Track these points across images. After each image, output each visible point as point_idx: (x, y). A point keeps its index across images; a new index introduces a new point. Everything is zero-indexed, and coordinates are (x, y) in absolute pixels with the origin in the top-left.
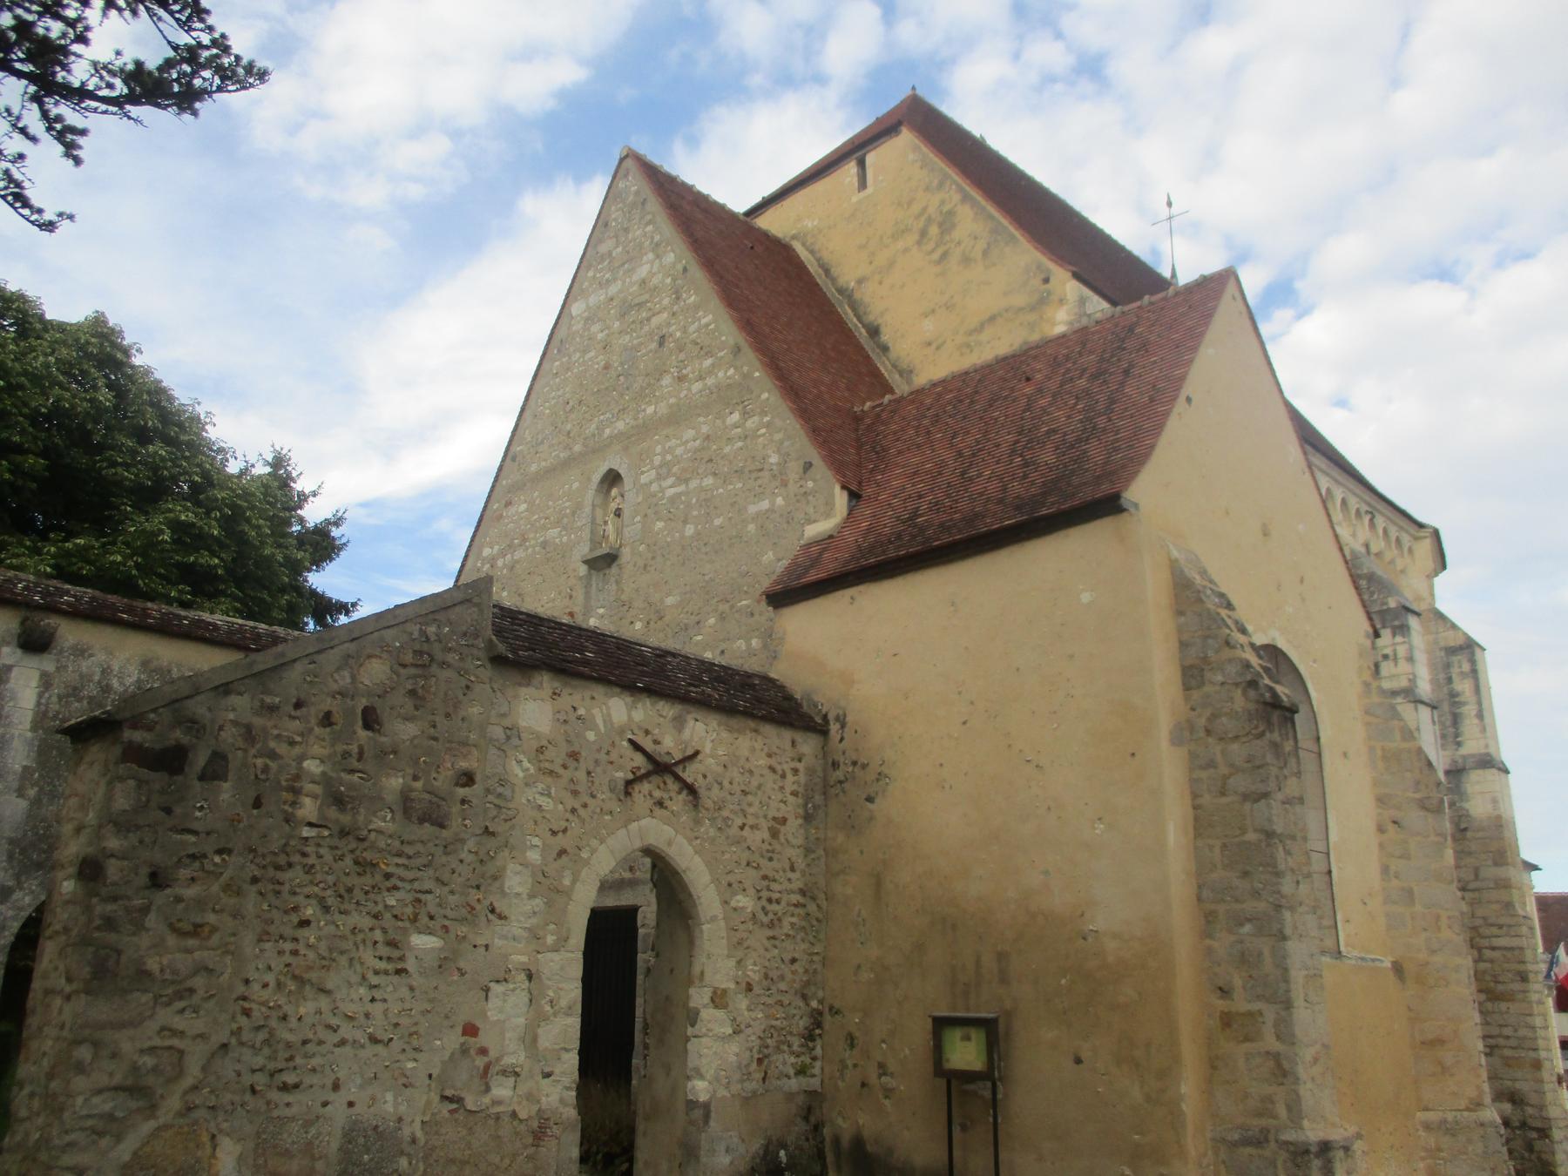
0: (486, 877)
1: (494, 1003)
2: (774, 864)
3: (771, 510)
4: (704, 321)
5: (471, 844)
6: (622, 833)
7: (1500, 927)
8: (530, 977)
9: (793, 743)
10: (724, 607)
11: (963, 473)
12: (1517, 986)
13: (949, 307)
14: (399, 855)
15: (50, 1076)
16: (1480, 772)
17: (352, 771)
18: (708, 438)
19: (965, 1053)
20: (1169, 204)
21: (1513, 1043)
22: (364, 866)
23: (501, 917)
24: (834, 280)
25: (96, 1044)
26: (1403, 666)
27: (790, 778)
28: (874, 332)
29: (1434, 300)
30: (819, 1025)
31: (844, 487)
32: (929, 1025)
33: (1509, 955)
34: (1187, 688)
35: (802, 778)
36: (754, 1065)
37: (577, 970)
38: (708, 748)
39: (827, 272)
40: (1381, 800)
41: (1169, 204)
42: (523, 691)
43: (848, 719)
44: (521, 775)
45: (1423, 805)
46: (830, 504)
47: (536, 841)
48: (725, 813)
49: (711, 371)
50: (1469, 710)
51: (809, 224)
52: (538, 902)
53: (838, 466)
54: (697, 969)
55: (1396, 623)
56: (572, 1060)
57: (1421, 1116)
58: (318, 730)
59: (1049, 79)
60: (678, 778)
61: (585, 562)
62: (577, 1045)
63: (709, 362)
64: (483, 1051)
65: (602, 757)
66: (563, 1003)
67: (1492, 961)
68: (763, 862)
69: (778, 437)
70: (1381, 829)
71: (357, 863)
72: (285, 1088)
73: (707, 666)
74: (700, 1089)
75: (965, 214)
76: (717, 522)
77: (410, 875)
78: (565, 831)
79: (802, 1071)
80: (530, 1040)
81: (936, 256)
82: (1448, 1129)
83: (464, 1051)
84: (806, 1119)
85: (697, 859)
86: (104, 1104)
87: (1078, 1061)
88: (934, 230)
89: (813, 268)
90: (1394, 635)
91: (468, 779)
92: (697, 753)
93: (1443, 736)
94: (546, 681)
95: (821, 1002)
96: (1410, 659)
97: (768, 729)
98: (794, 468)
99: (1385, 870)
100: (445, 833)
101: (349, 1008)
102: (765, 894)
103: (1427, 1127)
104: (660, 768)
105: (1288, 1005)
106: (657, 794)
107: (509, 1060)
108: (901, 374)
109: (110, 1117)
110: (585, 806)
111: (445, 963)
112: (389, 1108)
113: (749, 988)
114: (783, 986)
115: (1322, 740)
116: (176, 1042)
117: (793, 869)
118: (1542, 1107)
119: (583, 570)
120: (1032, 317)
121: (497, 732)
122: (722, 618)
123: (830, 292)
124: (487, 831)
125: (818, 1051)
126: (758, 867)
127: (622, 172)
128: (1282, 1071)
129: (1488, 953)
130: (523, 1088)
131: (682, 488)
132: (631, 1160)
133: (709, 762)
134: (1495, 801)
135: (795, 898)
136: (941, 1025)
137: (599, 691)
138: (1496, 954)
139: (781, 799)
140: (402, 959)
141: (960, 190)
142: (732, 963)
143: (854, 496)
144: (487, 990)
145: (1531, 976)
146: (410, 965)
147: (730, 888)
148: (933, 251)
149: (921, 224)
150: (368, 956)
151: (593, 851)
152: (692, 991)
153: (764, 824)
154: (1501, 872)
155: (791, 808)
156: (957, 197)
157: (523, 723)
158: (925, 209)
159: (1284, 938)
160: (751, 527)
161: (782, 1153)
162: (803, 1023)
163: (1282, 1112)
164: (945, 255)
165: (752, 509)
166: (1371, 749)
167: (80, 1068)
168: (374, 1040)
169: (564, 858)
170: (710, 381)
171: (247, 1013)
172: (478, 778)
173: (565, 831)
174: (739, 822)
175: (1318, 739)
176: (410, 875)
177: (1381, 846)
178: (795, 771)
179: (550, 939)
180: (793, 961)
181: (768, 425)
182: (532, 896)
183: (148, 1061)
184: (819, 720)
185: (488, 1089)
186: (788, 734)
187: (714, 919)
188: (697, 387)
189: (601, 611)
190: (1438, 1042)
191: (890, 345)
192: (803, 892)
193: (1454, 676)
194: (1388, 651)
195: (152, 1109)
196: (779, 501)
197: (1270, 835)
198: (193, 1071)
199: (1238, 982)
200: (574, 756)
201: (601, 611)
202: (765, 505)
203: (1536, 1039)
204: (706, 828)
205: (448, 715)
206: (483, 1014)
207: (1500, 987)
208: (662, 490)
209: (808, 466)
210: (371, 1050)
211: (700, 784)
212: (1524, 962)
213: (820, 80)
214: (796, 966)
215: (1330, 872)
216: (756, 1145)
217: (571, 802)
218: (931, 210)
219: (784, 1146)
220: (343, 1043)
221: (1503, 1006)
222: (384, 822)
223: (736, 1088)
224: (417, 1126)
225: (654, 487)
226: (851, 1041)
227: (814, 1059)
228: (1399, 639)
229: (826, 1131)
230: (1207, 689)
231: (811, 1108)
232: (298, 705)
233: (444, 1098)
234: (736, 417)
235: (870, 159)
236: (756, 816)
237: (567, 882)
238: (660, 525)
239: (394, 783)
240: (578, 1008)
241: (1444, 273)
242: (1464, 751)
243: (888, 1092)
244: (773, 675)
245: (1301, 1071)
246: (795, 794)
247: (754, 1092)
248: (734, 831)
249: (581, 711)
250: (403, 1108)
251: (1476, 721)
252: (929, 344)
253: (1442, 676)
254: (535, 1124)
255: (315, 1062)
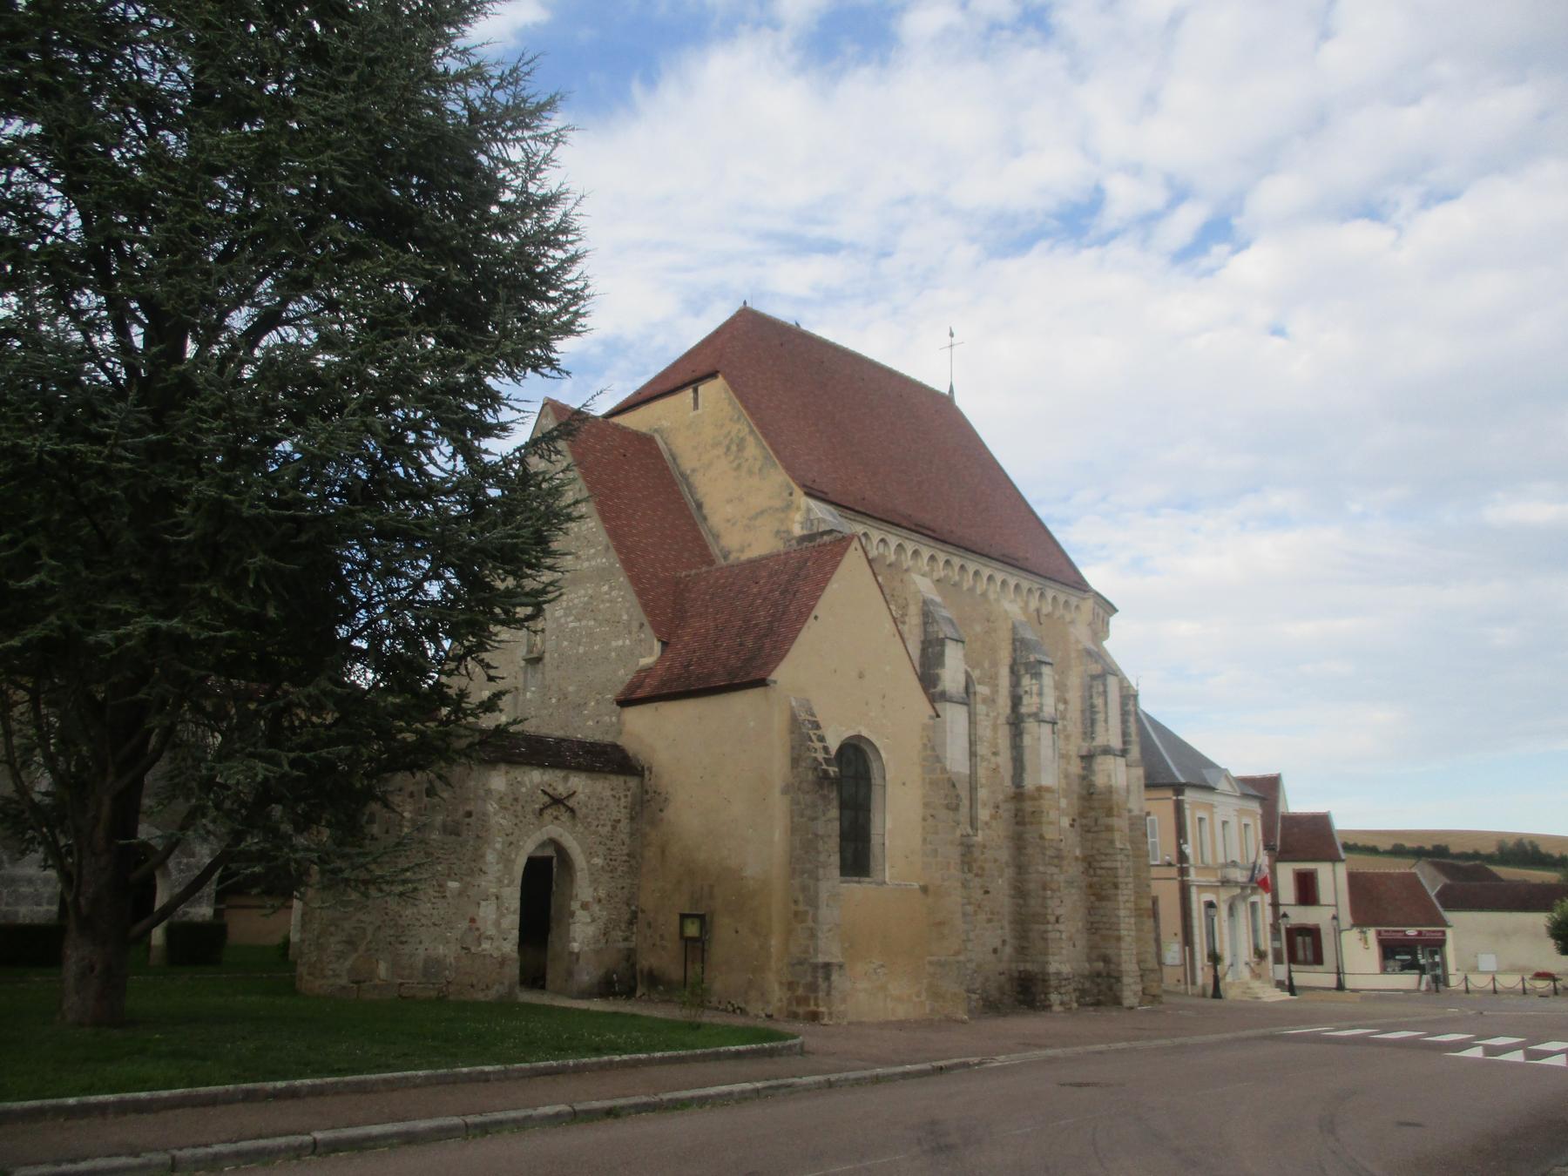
0: (478, 857)
1: (482, 909)
2: (614, 842)
3: (623, 646)
4: (590, 525)
5: (471, 843)
6: (538, 834)
7: (1106, 855)
8: (497, 898)
9: (625, 782)
10: (599, 697)
11: (715, 641)
12: (1112, 892)
13: (740, 499)
14: (442, 849)
15: (318, 938)
16: (1103, 757)
17: (422, 815)
18: (591, 597)
19: (692, 930)
20: (952, 335)
21: (1108, 926)
22: (428, 854)
23: (485, 873)
24: (678, 466)
25: (337, 926)
26: (1035, 699)
27: (623, 800)
28: (700, 506)
29: (1361, 237)
30: (636, 918)
31: (659, 640)
32: (677, 918)
33: (1110, 872)
34: (792, 768)
35: (629, 799)
36: (601, 937)
37: (518, 895)
38: (580, 789)
39: (674, 459)
40: (926, 805)
41: (952, 335)
42: (494, 773)
43: (654, 769)
44: (492, 810)
45: (948, 807)
46: (652, 648)
47: (499, 839)
48: (589, 820)
49: (594, 557)
50: (1100, 717)
51: (665, 424)
52: (500, 866)
53: (656, 627)
54: (574, 892)
55: (1033, 671)
56: (516, 933)
57: (929, 958)
58: (409, 800)
59: (994, 27)
60: (565, 805)
61: (525, 660)
62: (518, 927)
63: (592, 551)
64: (478, 929)
65: (529, 799)
66: (512, 909)
67: (1100, 876)
68: (608, 842)
69: (627, 605)
70: (924, 819)
71: (426, 853)
72: (402, 943)
73: (581, 744)
74: (575, 946)
75: (750, 440)
76: (596, 648)
77: (446, 857)
78: (512, 834)
79: (626, 939)
80: (497, 924)
81: (735, 465)
82: (941, 964)
83: (470, 929)
84: (628, 961)
85: (575, 842)
86: (340, 947)
87: (737, 932)
88: (734, 448)
89: (666, 456)
90: (1032, 679)
91: (469, 814)
92: (575, 792)
93: (1085, 733)
94: (503, 767)
95: (637, 907)
96: (1040, 694)
97: (612, 777)
98: (635, 625)
99: (924, 840)
100: (460, 839)
101: (425, 912)
102: (609, 857)
103: (931, 963)
104: (556, 801)
105: (817, 908)
106: (555, 813)
107: (489, 933)
108: (713, 535)
109: (342, 952)
110: (521, 822)
111: (461, 893)
112: (441, 951)
113: (600, 901)
114: (617, 900)
115: (887, 778)
116: (362, 925)
117: (623, 844)
118: (1119, 964)
119: (523, 663)
120: (782, 515)
121: (482, 793)
122: (598, 702)
123: (676, 474)
124: (478, 837)
125: (635, 930)
126: (605, 844)
127: (544, 413)
128: (813, 935)
129: (1099, 872)
130: (495, 944)
131: (577, 624)
132: (545, 980)
133: (581, 797)
134: (1109, 776)
135: (625, 858)
136: (683, 917)
137: (527, 769)
138: (1103, 871)
139: (618, 810)
140: (444, 892)
141: (749, 426)
142: (592, 889)
143: (665, 644)
144: (479, 904)
145: (1121, 886)
146: (448, 894)
147: (590, 855)
148: (733, 461)
149: (727, 442)
150: (431, 891)
151: (525, 842)
152: (572, 903)
153: (609, 823)
154: (1109, 821)
155: (623, 814)
156: (747, 430)
157: (493, 787)
158: (729, 433)
159: (818, 880)
160: (613, 654)
161: (615, 976)
162: (627, 917)
163: (811, 951)
164: (739, 466)
165: (614, 644)
166: (924, 779)
167: (332, 934)
168: (435, 925)
169: (512, 846)
170: (593, 563)
171: (387, 914)
172: (474, 814)
173: (512, 834)
174: (595, 823)
175: (884, 778)
176: (446, 857)
177: (924, 828)
178: (626, 796)
179: (506, 882)
180: (623, 888)
181: (623, 597)
182: (498, 863)
183: (354, 932)
184: (640, 768)
185: (480, 945)
186: (622, 779)
187: (582, 870)
188: (586, 564)
189: (533, 689)
190: (941, 924)
191: (708, 517)
192: (628, 855)
193: (1094, 694)
194: (1027, 689)
195: (356, 950)
196: (627, 642)
197: (816, 835)
198: (369, 937)
199: (801, 898)
200: (516, 800)
201: (533, 689)
202: (620, 643)
203: (1119, 924)
204: (580, 828)
205: (461, 787)
206: (478, 915)
207: (1104, 893)
208: (567, 623)
209: (642, 625)
210: (432, 929)
211: (576, 807)
212: (1116, 877)
213: (775, 25)
214: (625, 890)
215: (884, 844)
216: (602, 972)
217: (515, 821)
218: (733, 434)
219: (615, 972)
220: (423, 925)
221: (1104, 903)
222: (435, 836)
223: (592, 946)
224: (452, 959)
225: (563, 620)
226: (649, 925)
227: (633, 933)
228: (1034, 681)
229: (638, 967)
230: (800, 769)
231: (630, 956)
232: (400, 790)
233: (463, 948)
234: (606, 588)
235: (701, 389)
236: (605, 820)
237: (513, 856)
238: (566, 643)
239: (439, 819)
240: (519, 912)
241: (1370, 210)
242: (1094, 744)
243: (664, 948)
244: (619, 743)
245: (820, 935)
246: (625, 807)
247: (601, 949)
248: (593, 828)
249: (519, 779)
250: (447, 952)
251: (1103, 724)
252: (728, 521)
253: (1087, 694)
254: (500, 959)
255: (413, 932)
